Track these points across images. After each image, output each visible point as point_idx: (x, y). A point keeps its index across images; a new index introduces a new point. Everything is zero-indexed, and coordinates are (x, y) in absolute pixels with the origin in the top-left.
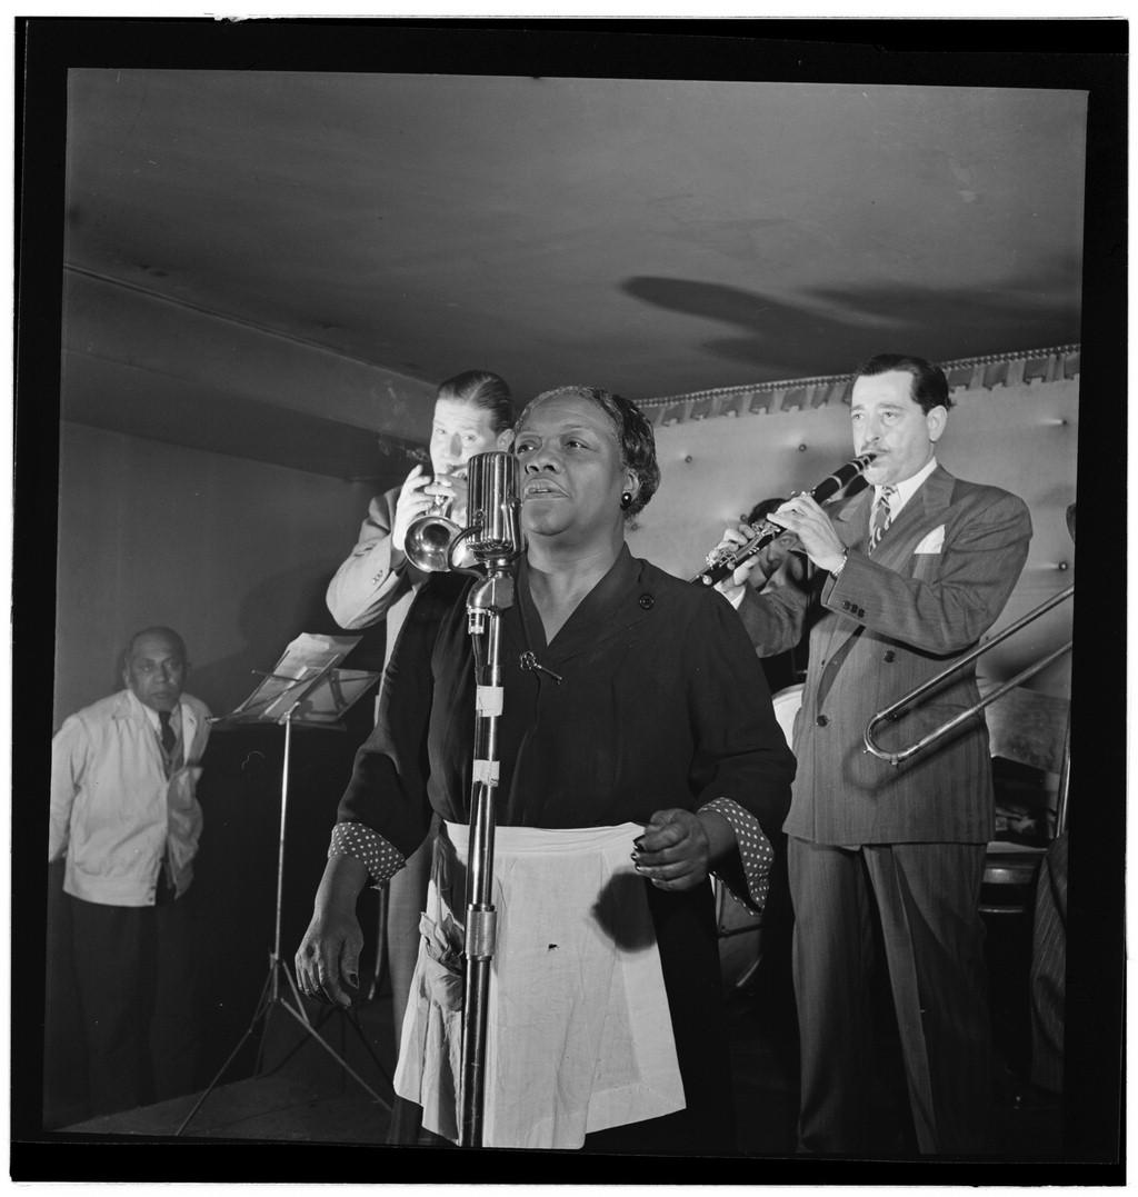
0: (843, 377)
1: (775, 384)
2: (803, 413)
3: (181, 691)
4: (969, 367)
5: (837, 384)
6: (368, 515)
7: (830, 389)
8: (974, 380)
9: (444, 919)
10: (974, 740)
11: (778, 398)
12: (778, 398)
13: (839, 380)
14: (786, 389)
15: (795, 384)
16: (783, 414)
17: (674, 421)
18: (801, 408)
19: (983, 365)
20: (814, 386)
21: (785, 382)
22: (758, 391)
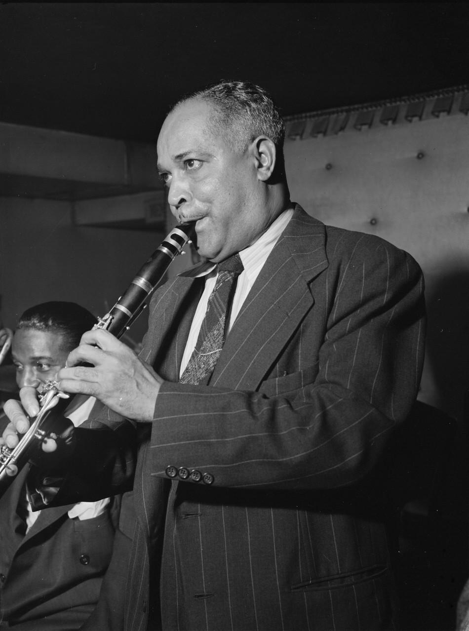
0: (356, 106)
1: (308, 114)
2: (423, 122)
3: (97, 398)
4: (451, 94)
5: (353, 112)
6: (123, 494)
7: (346, 120)
8: (455, 107)
9: (211, 260)
10: (328, 230)
11: (309, 129)
12: (309, 129)
13: (354, 109)
14: (316, 118)
15: (321, 115)
16: (434, 120)
17: (390, 123)
18: (421, 118)
19: (461, 93)
20: (335, 115)
21: (315, 113)
22: (296, 121)
